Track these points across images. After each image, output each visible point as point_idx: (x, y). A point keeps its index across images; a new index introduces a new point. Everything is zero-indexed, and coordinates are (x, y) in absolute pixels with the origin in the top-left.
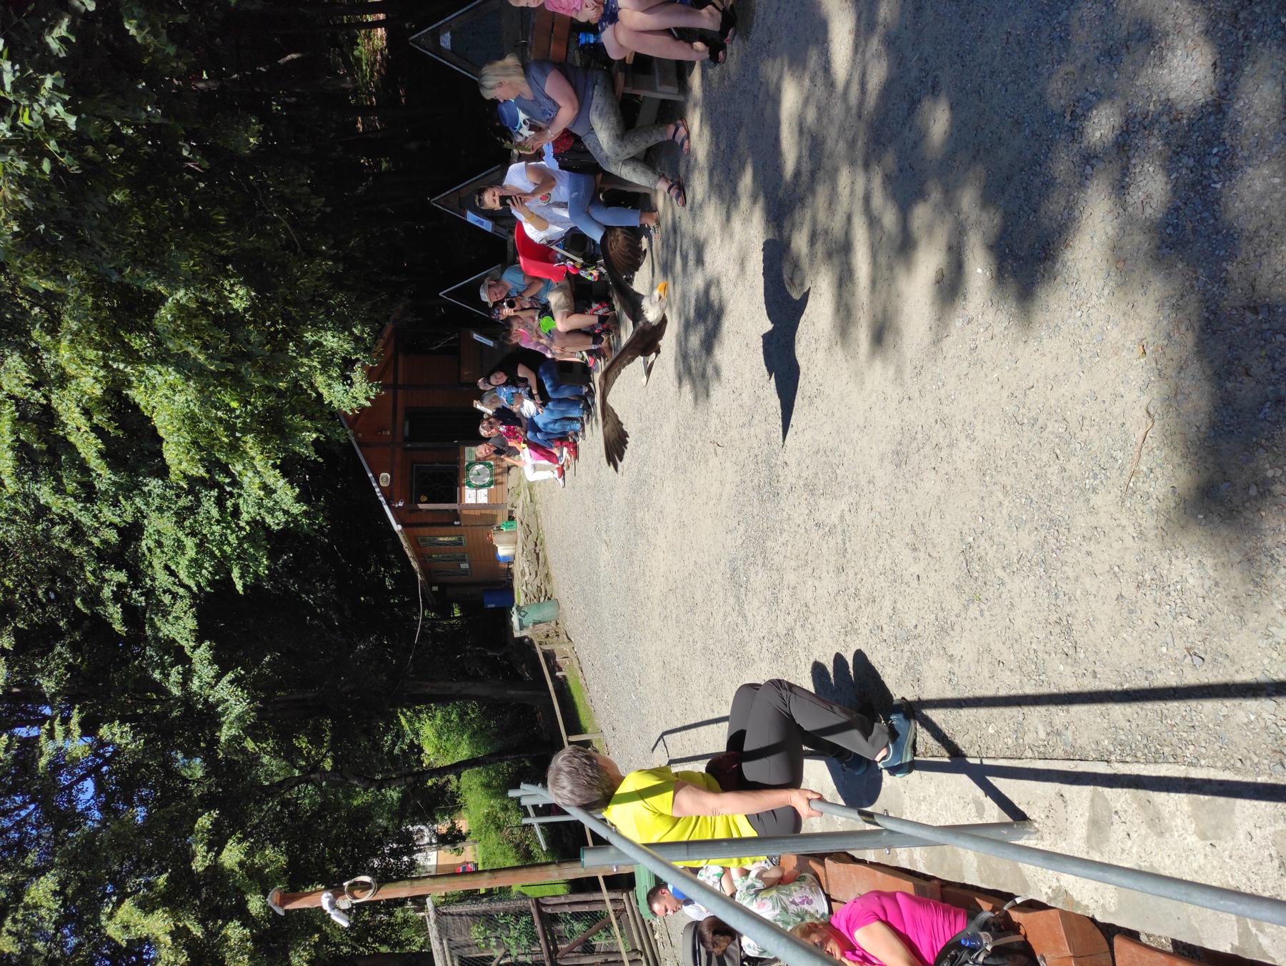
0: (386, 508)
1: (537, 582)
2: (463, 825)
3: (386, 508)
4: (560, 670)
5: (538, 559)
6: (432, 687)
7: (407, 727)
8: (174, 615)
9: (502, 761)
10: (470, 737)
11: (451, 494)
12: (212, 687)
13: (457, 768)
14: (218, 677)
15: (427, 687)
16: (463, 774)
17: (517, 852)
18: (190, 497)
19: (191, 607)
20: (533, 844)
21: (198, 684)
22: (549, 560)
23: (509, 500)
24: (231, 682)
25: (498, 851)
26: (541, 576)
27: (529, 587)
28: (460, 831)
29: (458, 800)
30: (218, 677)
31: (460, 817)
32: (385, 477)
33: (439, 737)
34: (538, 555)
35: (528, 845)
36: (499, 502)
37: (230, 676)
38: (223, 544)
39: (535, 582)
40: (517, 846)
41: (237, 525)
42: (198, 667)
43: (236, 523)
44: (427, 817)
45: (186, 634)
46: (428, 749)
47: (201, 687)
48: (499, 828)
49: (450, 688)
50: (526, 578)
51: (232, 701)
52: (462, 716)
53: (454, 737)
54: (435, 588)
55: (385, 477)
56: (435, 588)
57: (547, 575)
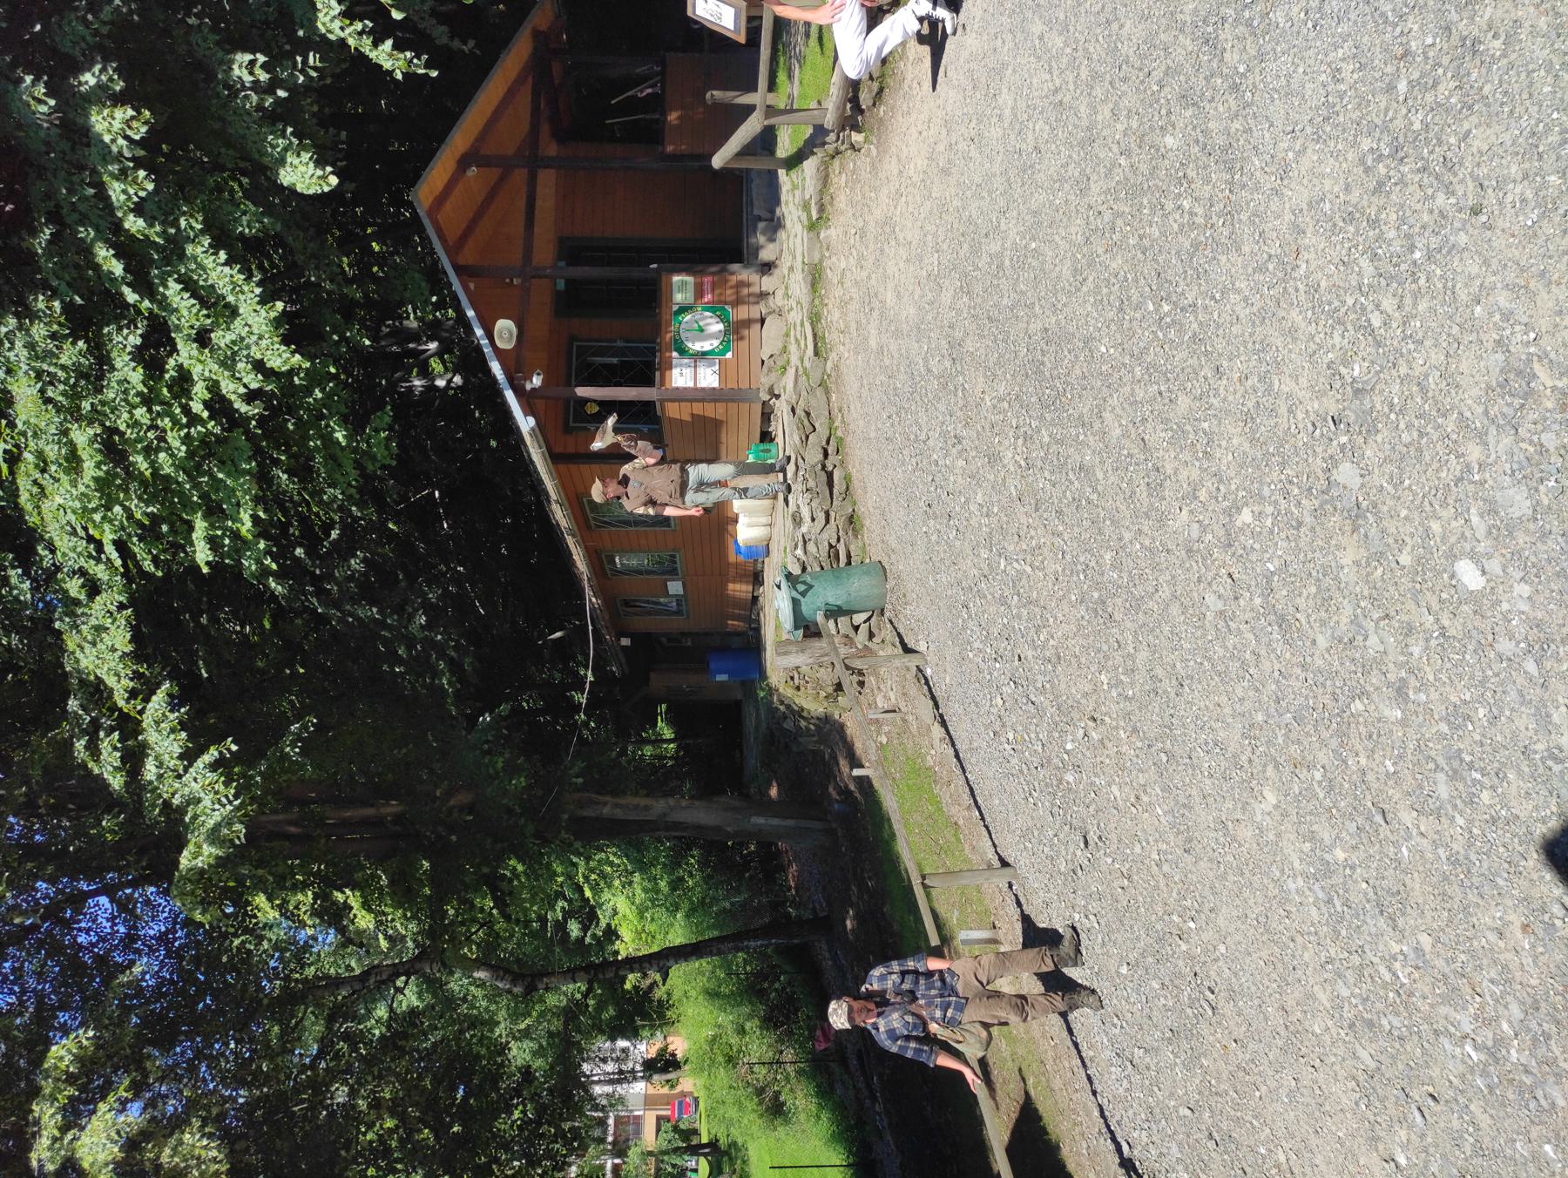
0: (510, 396)
1: (830, 535)
2: (679, 1045)
3: (510, 396)
4: (855, 762)
5: (830, 483)
6: (616, 805)
7: (52, 369)
8: (93, 622)
9: (738, 950)
10: (687, 916)
11: (646, 369)
12: (179, 777)
13: (664, 959)
14: (189, 757)
15: (605, 804)
16: (672, 972)
17: (760, 1103)
18: (81, 343)
19: (121, 607)
20: (786, 1089)
21: (154, 770)
22: (855, 483)
23: (765, 381)
24: (213, 766)
25: (730, 1100)
26: (838, 520)
27: (811, 547)
28: (674, 1055)
29: (669, 1013)
30: (189, 757)
31: (676, 1033)
32: (505, 328)
33: (641, 917)
34: (830, 476)
35: (778, 1094)
36: (744, 385)
37: (212, 754)
38: (158, 450)
39: (825, 536)
40: (760, 1092)
41: (186, 410)
42: (151, 736)
43: (181, 406)
44: (626, 1027)
45: (113, 661)
46: (626, 933)
47: (160, 777)
48: (731, 1060)
49: (647, 808)
50: (804, 529)
51: (207, 801)
52: (676, 884)
53: (662, 914)
54: (625, 642)
55: (505, 328)
56: (625, 642)
57: (851, 519)
